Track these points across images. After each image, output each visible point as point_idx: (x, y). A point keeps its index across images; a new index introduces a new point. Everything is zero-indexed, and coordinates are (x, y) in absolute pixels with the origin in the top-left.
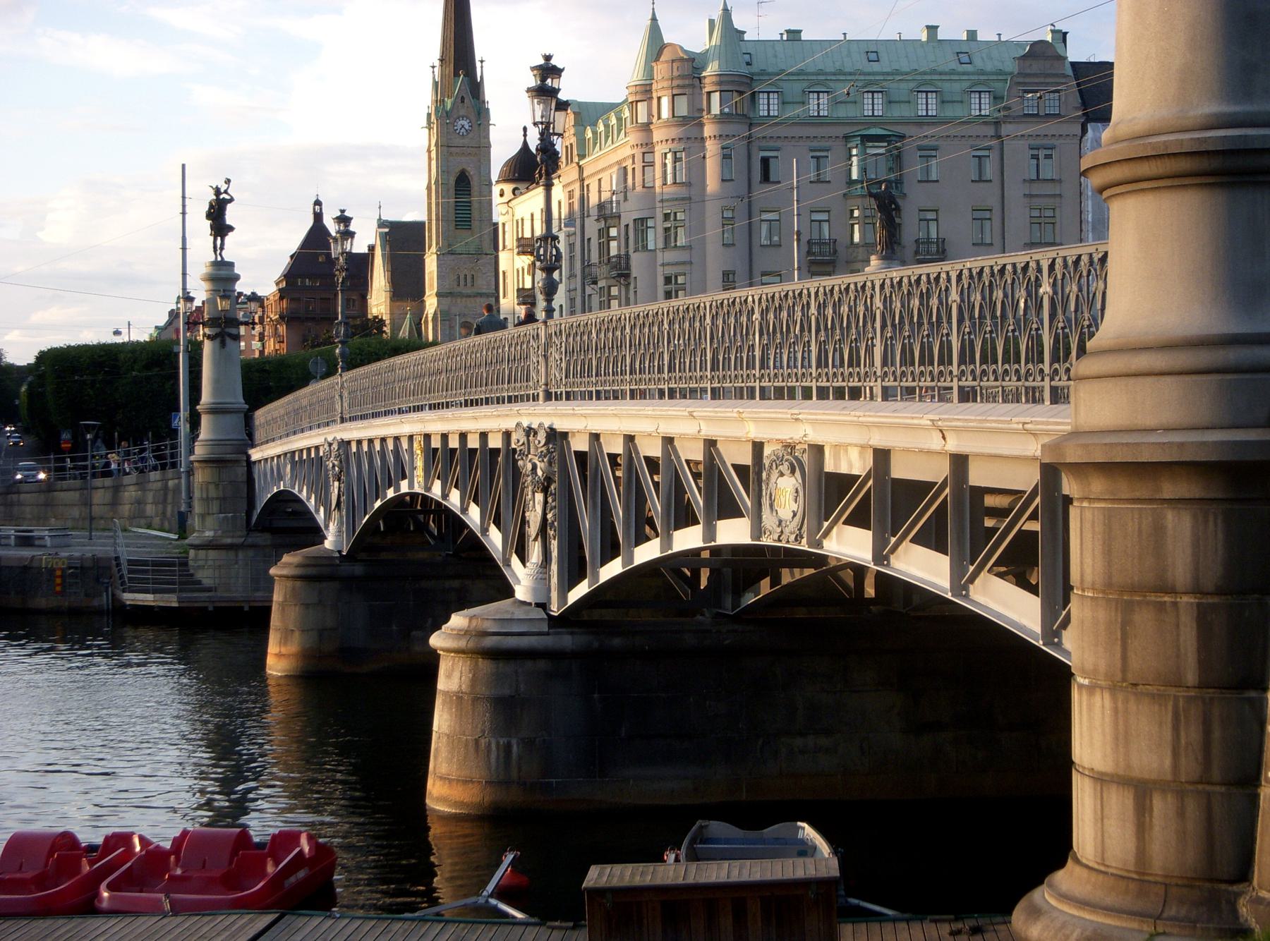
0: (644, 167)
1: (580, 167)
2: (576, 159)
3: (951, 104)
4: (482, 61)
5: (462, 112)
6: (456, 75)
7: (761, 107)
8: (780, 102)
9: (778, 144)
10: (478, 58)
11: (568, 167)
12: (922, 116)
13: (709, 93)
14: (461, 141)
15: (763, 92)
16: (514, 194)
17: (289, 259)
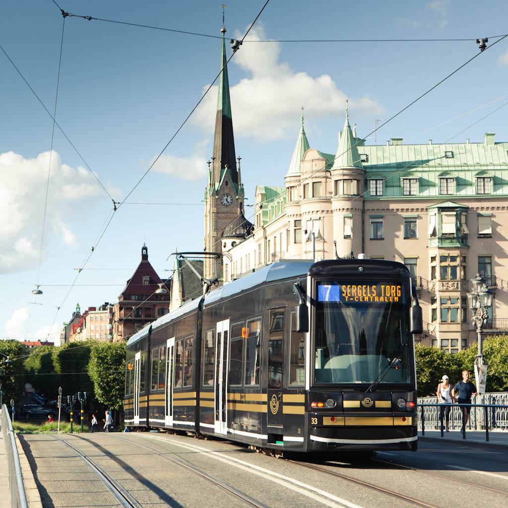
0: (295, 230)
1: (264, 229)
2: (262, 224)
3: (392, 188)
4: (239, 159)
5: (227, 191)
6: (223, 167)
7: (371, 190)
8: (384, 186)
9: (383, 214)
10: (237, 157)
11: (258, 229)
12: (373, 196)
13: (336, 181)
14: (226, 209)
15: (373, 180)
16: (232, 245)
17: (126, 283)
